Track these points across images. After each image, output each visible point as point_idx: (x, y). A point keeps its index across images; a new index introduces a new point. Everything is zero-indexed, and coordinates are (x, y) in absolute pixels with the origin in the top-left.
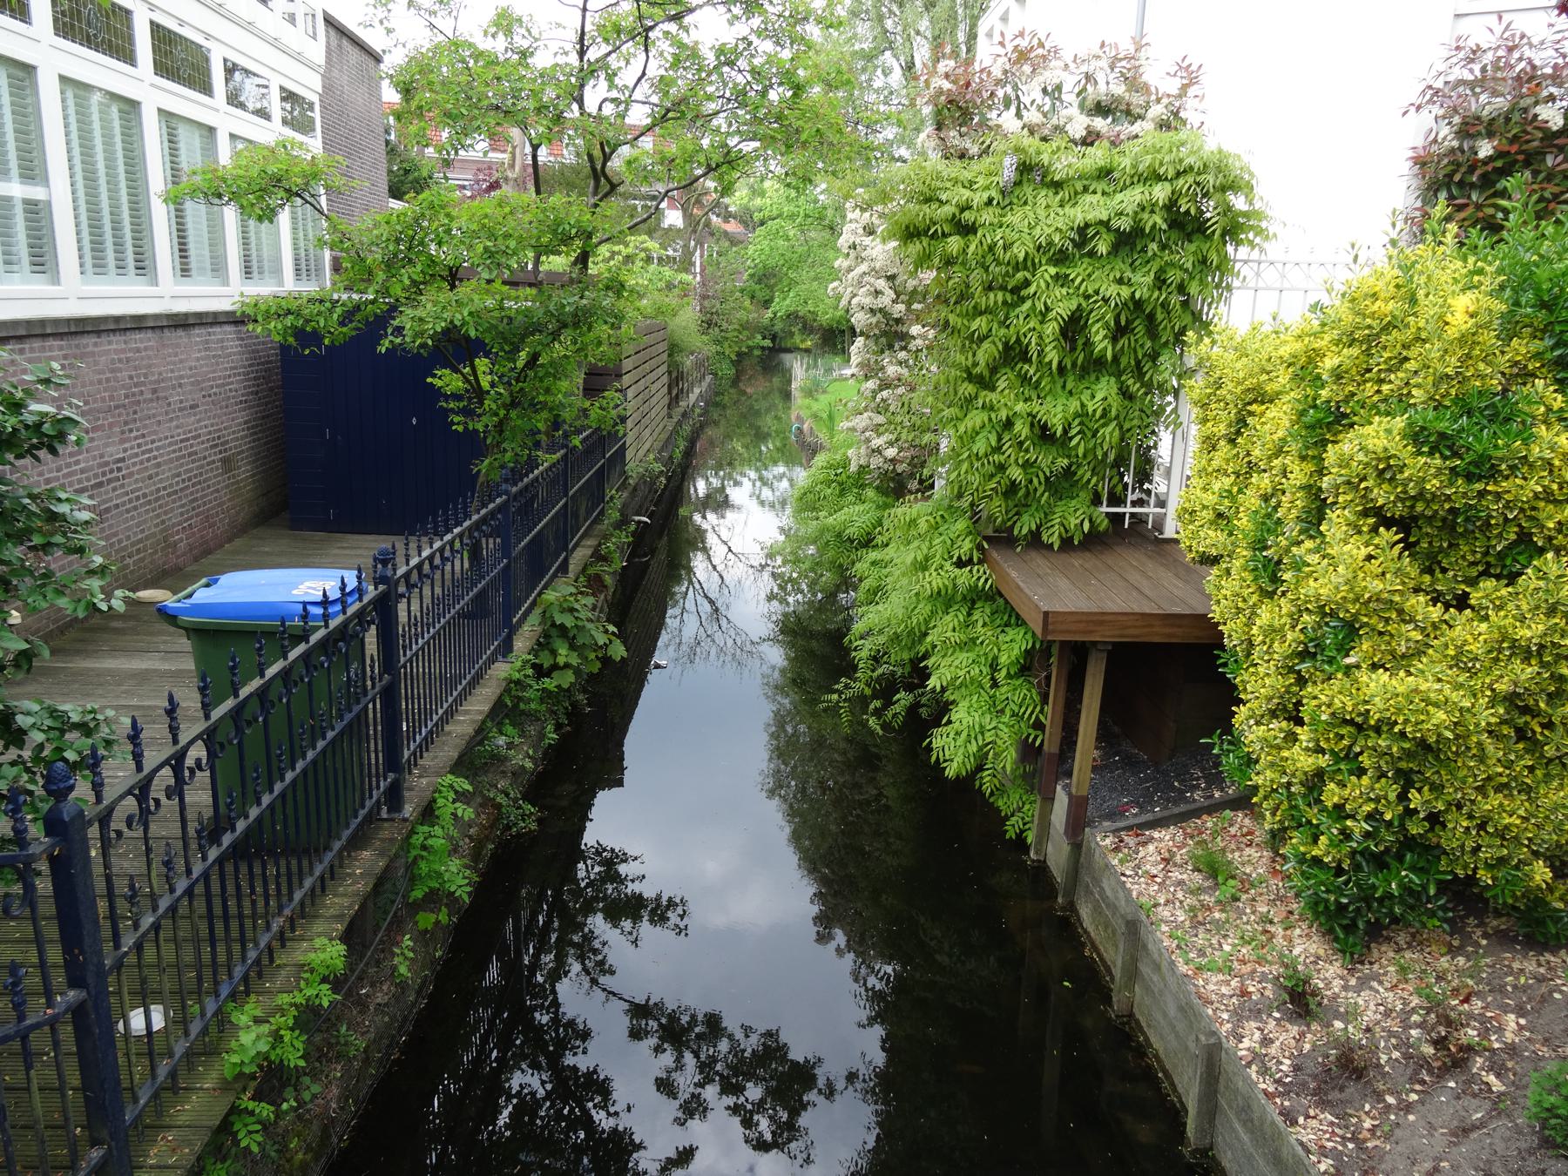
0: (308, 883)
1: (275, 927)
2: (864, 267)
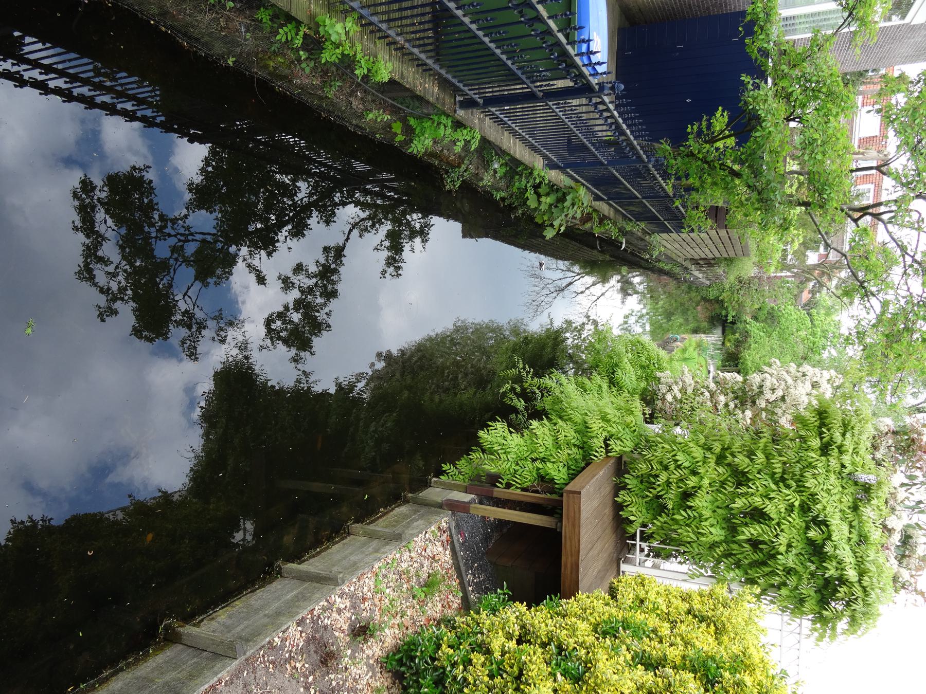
0: (423, 56)
1: (399, 39)
2: (790, 381)
